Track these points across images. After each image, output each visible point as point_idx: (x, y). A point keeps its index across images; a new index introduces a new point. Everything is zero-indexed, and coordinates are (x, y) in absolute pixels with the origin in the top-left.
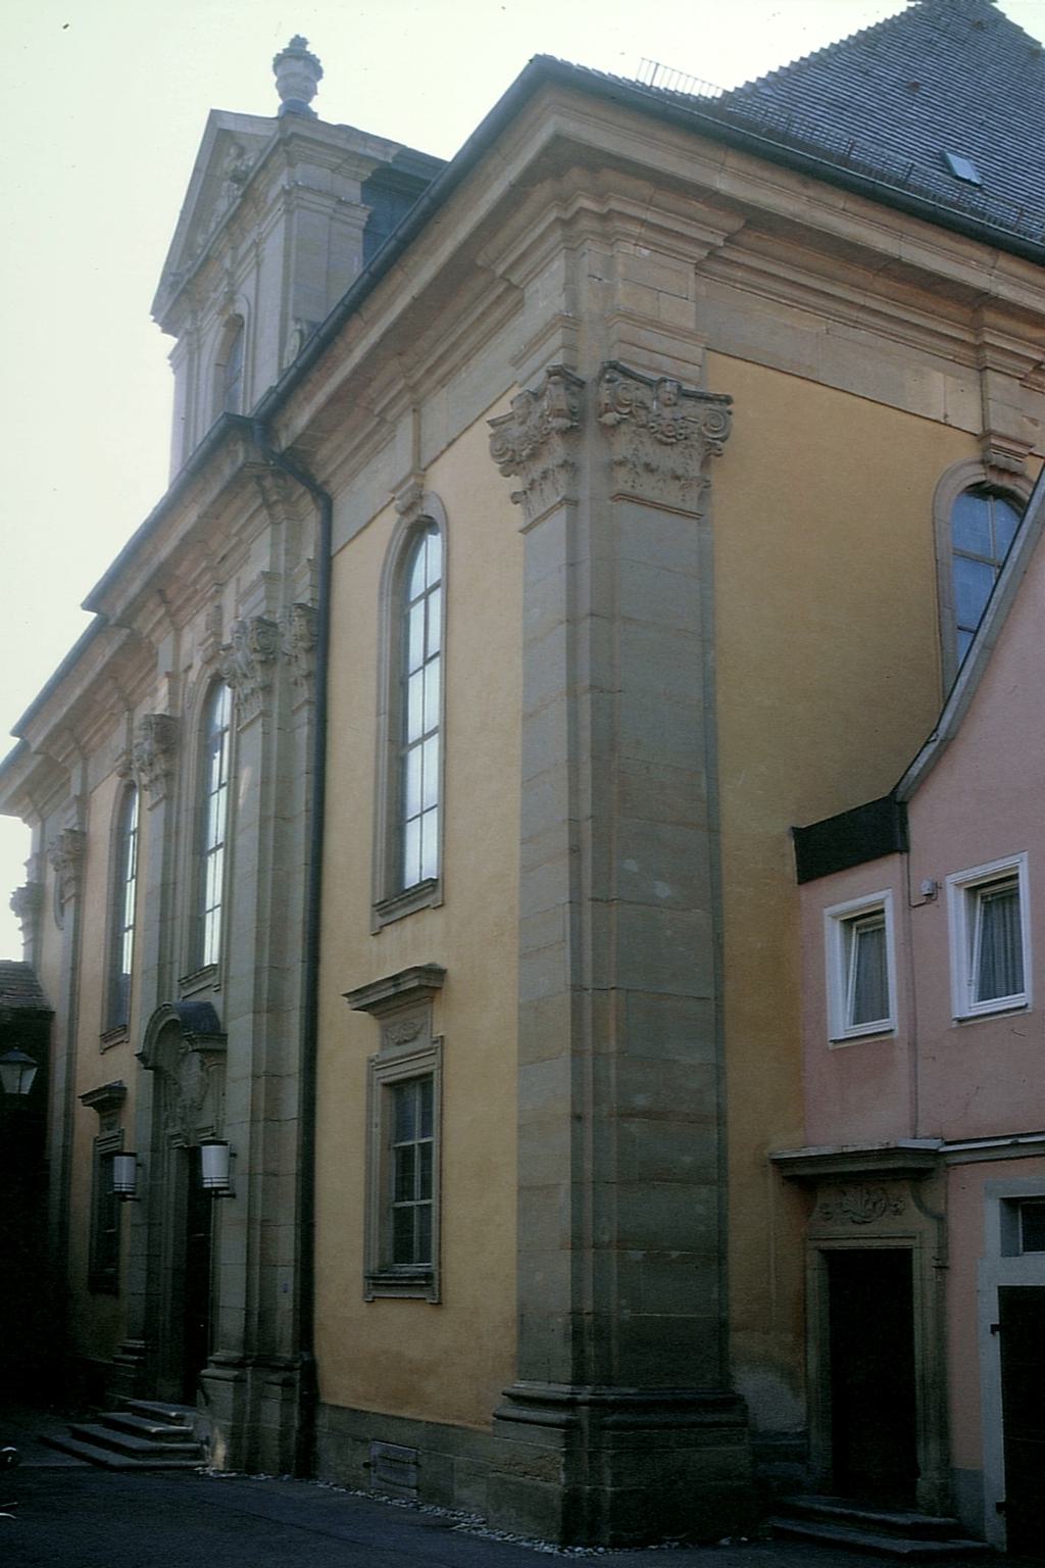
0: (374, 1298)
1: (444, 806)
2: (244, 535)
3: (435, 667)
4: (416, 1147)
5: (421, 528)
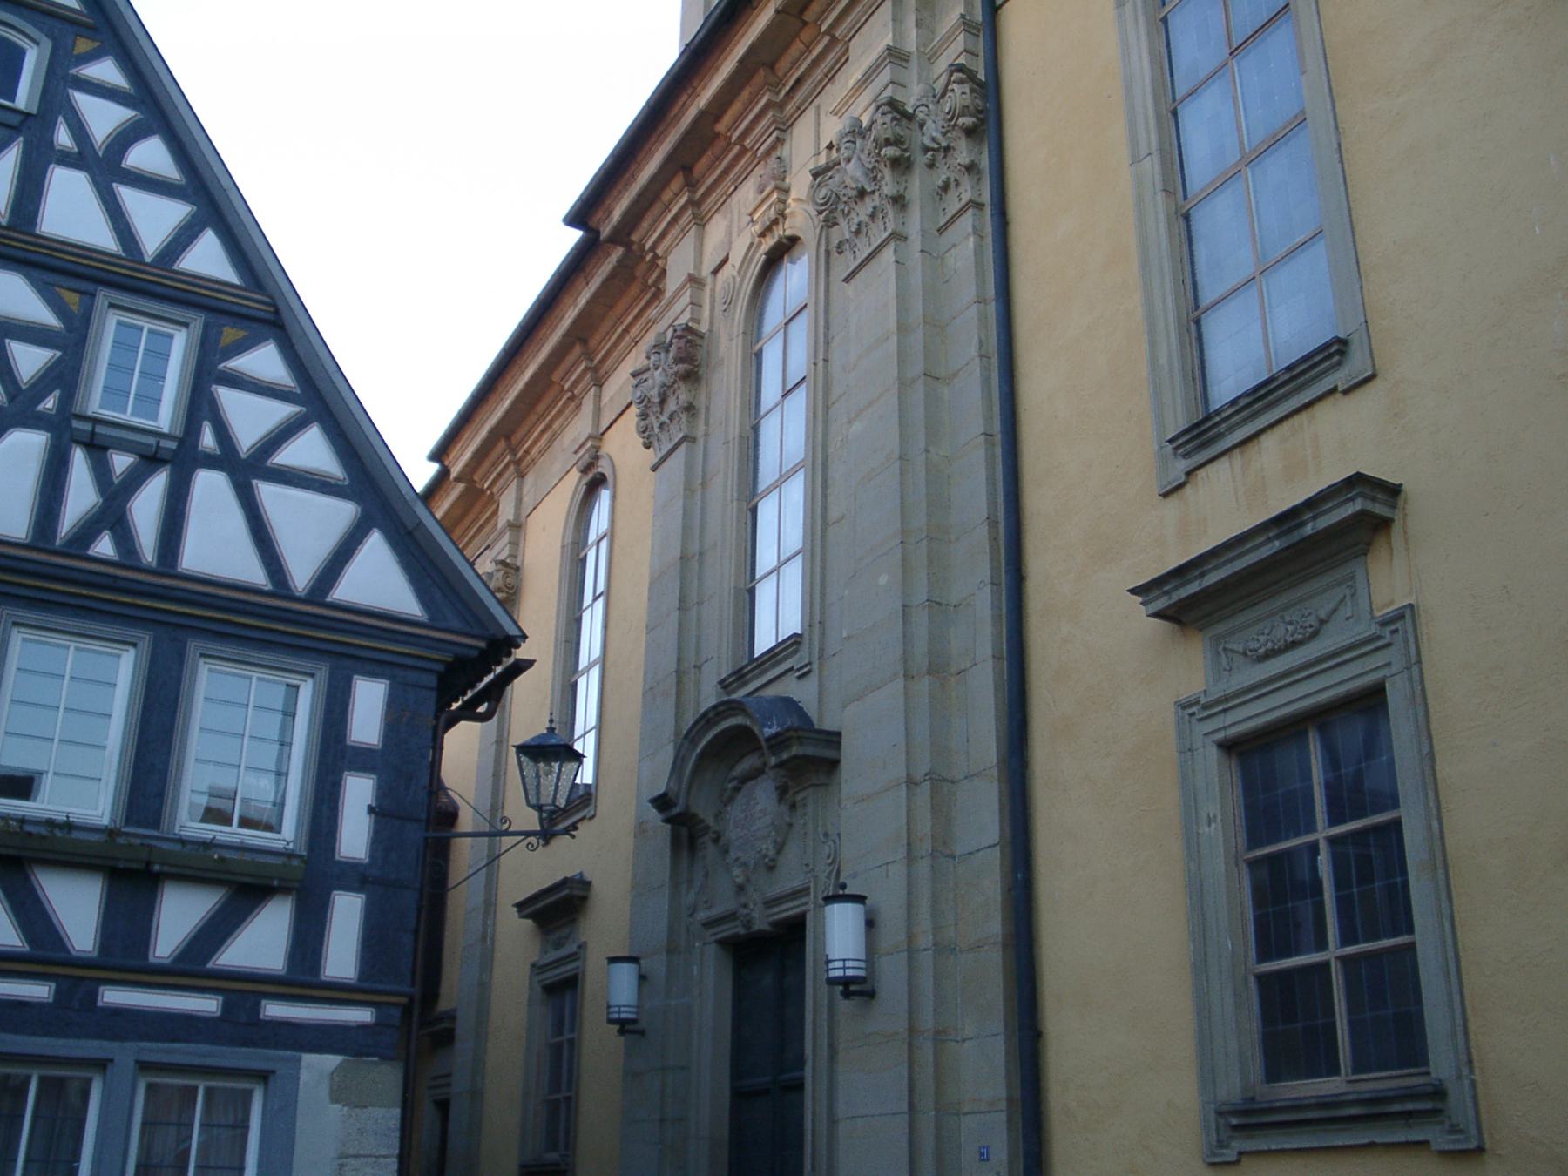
0: (1241, 1154)
1: (600, 728)
2: (748, 142)
3: (600, 603)
4: (1323, 846)
5: (595, 484)
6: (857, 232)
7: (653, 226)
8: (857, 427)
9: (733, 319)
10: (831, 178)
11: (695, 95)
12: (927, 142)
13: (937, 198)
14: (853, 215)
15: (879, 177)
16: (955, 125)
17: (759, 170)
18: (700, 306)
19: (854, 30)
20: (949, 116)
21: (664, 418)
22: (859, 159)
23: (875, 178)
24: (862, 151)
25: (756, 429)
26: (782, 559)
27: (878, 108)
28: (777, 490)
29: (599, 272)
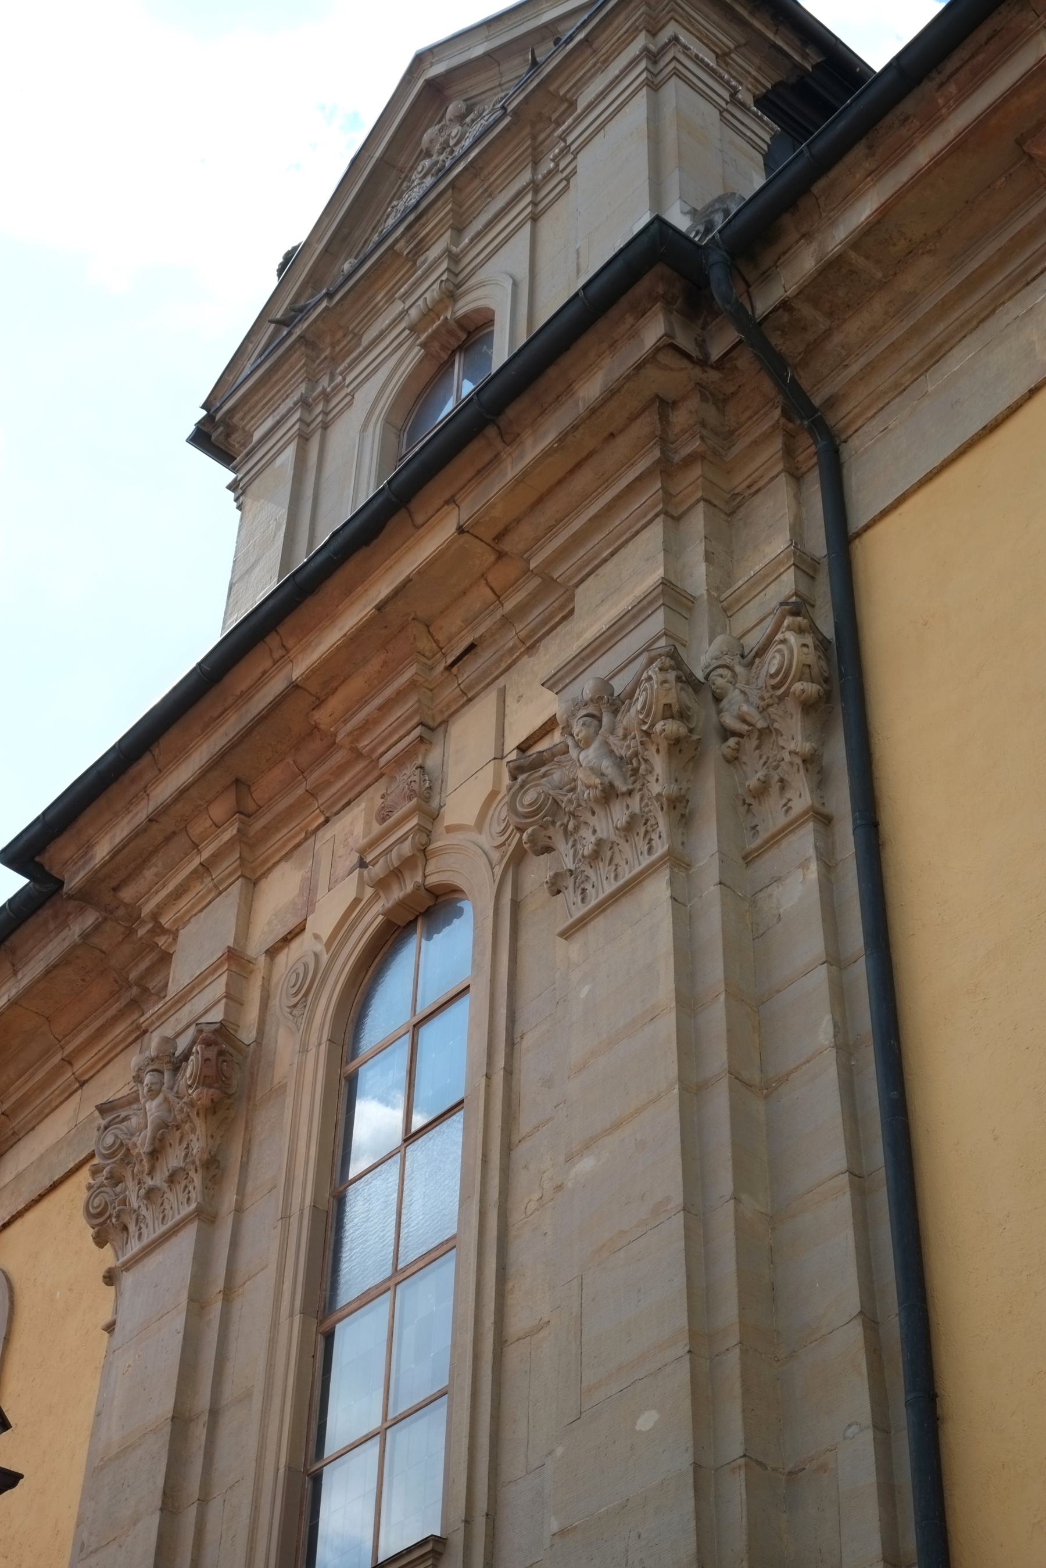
6: (596, 855)
7: (161, 879)
8: (587, 1164)
9: (310, 1022)
10: (544, 776)
11: (286, 657)
12: (730, 721)
13: (743, 809)
14: (586, 833)
15: (642, 771)
16: (786, 694)
17: (380, 788)
18: (242, 1005)
19: (588, 569)
20: (774, 682)
21: (158, 1180)
22: (606, 743)
23: (635, 771)
24: (612, 731)
25: (340, 1201)
26: (391, 1416)
27: (651, 661)
28: (389, 1294)
29: (41, 955)
